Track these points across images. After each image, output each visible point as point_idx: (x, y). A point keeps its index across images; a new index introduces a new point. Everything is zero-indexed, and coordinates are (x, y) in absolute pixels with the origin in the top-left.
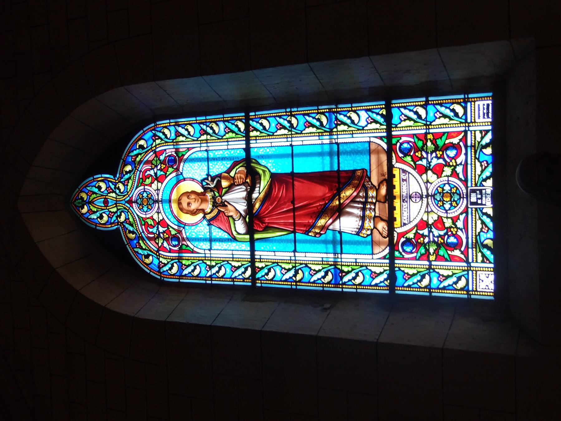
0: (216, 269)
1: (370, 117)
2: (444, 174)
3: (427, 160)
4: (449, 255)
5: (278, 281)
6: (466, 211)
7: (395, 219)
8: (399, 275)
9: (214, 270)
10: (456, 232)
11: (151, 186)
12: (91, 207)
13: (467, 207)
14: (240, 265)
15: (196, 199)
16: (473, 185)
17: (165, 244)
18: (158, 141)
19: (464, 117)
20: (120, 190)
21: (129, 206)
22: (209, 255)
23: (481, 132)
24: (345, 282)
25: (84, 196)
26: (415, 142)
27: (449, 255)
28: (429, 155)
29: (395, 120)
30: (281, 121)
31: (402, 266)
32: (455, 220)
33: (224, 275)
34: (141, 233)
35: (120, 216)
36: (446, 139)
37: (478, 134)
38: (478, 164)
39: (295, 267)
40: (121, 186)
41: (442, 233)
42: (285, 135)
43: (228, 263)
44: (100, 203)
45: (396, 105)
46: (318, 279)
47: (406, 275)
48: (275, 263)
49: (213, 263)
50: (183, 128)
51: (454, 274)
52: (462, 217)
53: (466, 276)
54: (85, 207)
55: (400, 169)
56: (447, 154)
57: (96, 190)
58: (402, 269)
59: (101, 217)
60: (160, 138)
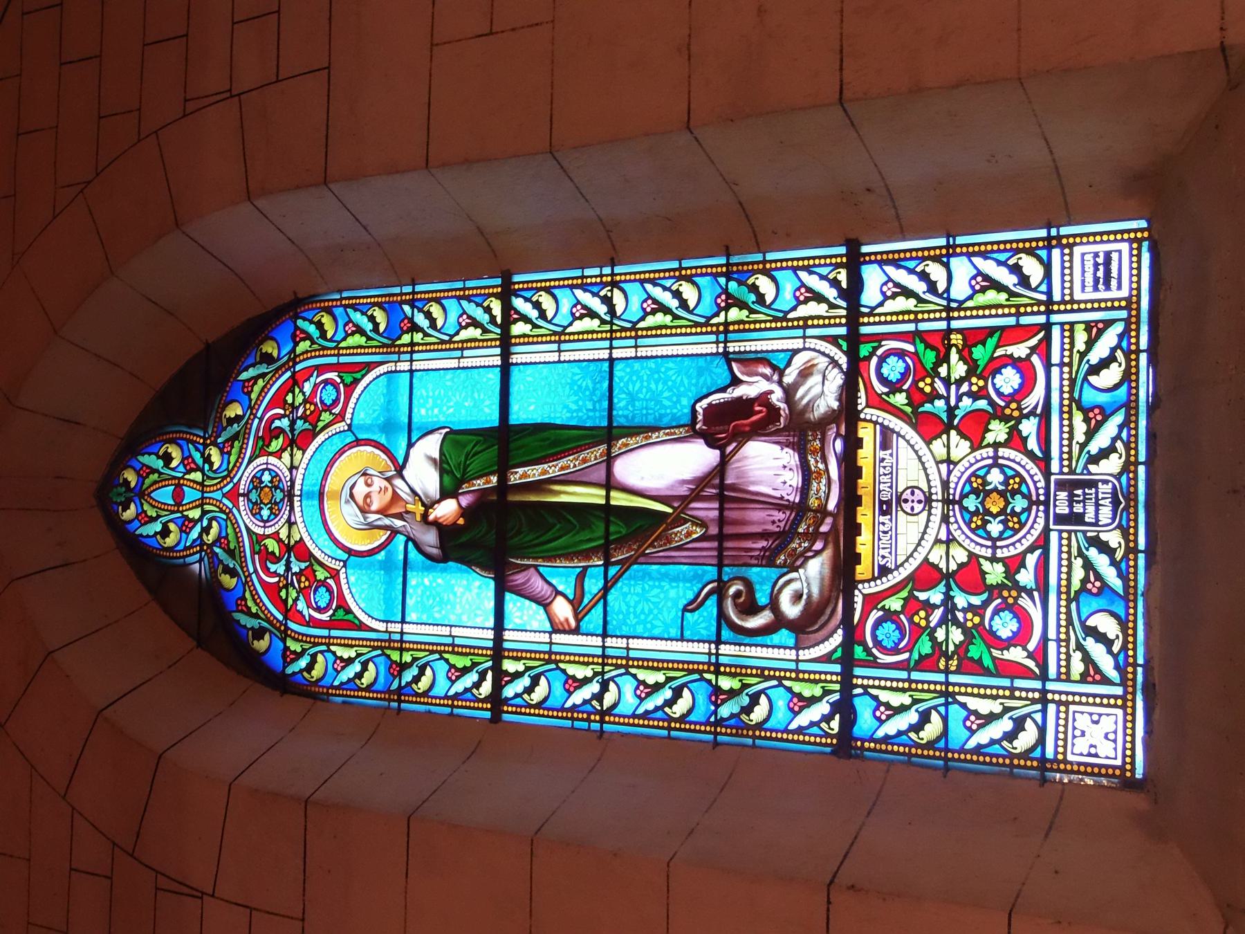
1: (890, 280)
2: (990, 438)
3: (948, 403)
4: (994, 659)
5: (440, 698)
6: (1043, 543)
7: (857, 559)
8: (863, 707)
9: (408, 676)
10: (1016, 599)
11: (280, 458)
12: (146, 507)
13: (1046, 531)
14: (469, 664)
16: (1066, 470)
17: (301, 605)
18: (304, 346)
19: (1044, 288)
20: (211, 464)
21: (230, 505)
22: (397, 637)
23: (1088, 326)
24: (723, 719)
25: (131, 477)
26: (916, 353)
27: (994, 659)
28: (953, 388)
29: (870, 296)
30: (657, 292)
31: (871, 682)
32: (1014, 565)
33: (546, 699)
34: (250, 575)
35: (206, 530)
36: (997, 346)
37: (1079, 329)
38: (1078, 417)
39: (603, 673)
40: (216, 457)
41: (976, 600)
42: (909, 312)
43: (442, 658)
44: (165, 495)
45: (790, 264)
46: (812, 724)
47: (882, 709)
48: (774, 678)
49: (407, 658)
50: (478, 305)
51: (1007, 710)
52: (1031, 560)
53: (942, 709)
54: (132, 506)
55: (876, 423)
56: (994, 385)
57: (159, 464)
58: (873, 692)
59: (165, 532)
60: (308, 337)
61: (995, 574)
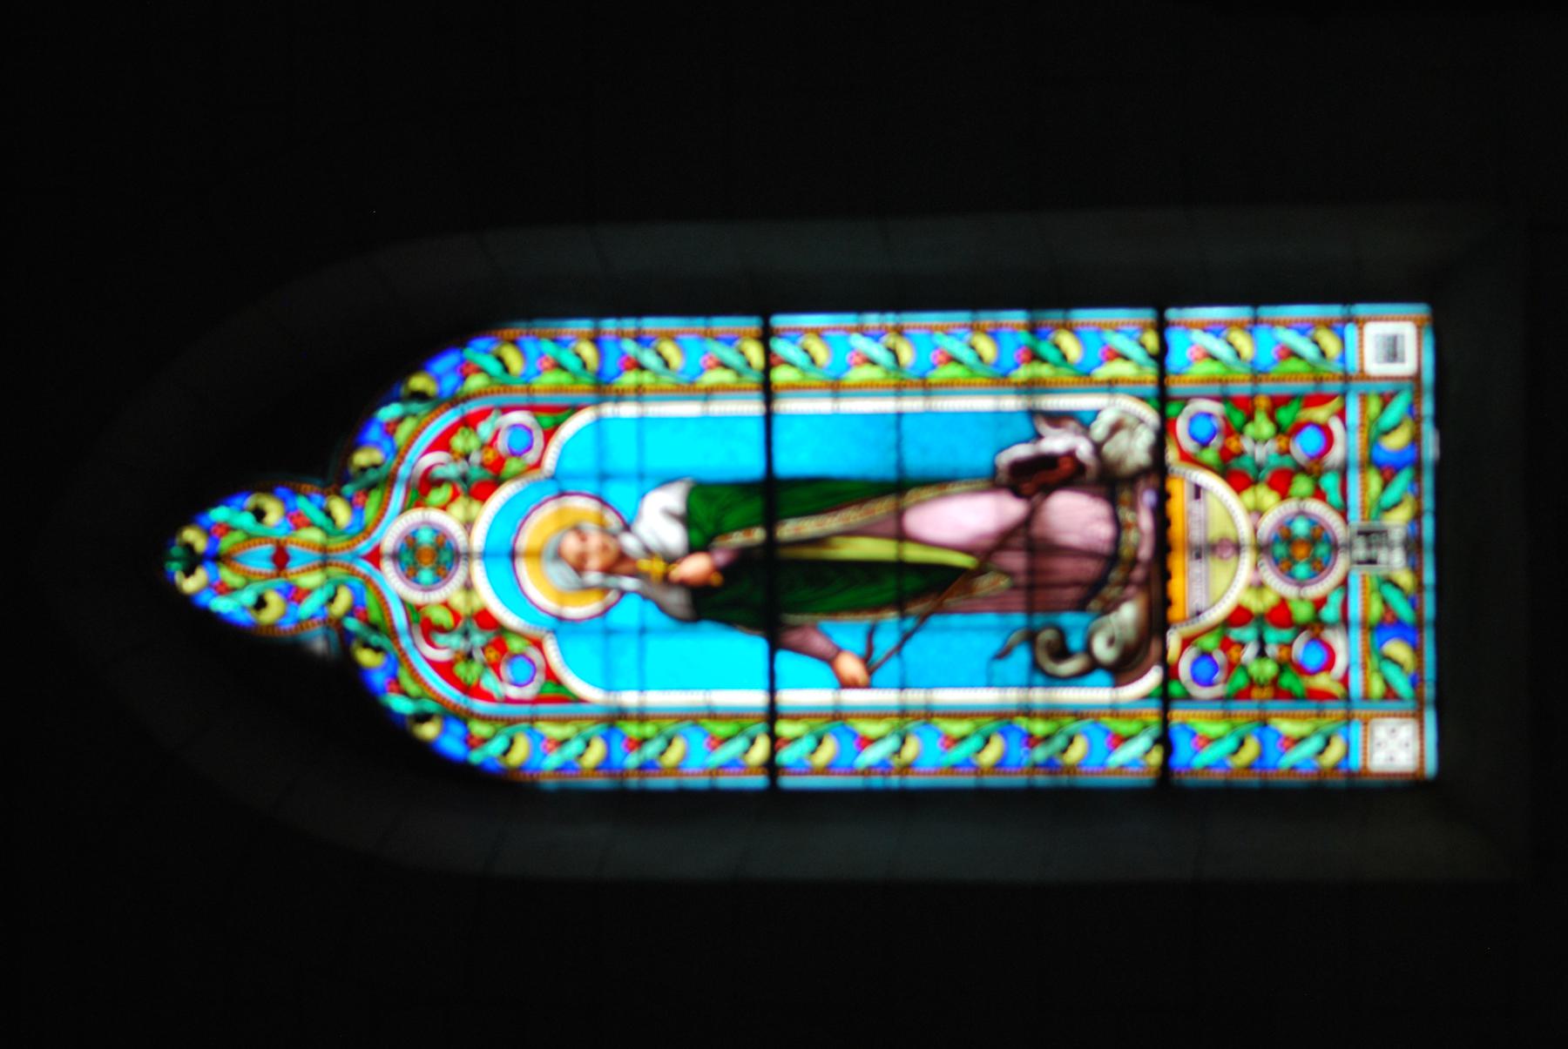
0: (1392, 672)
6: (1344, 584)
9: (651, 750)
15: (546, 550)
32: (1320, 603)
59: (261, 603)
61: (1302, 612)
